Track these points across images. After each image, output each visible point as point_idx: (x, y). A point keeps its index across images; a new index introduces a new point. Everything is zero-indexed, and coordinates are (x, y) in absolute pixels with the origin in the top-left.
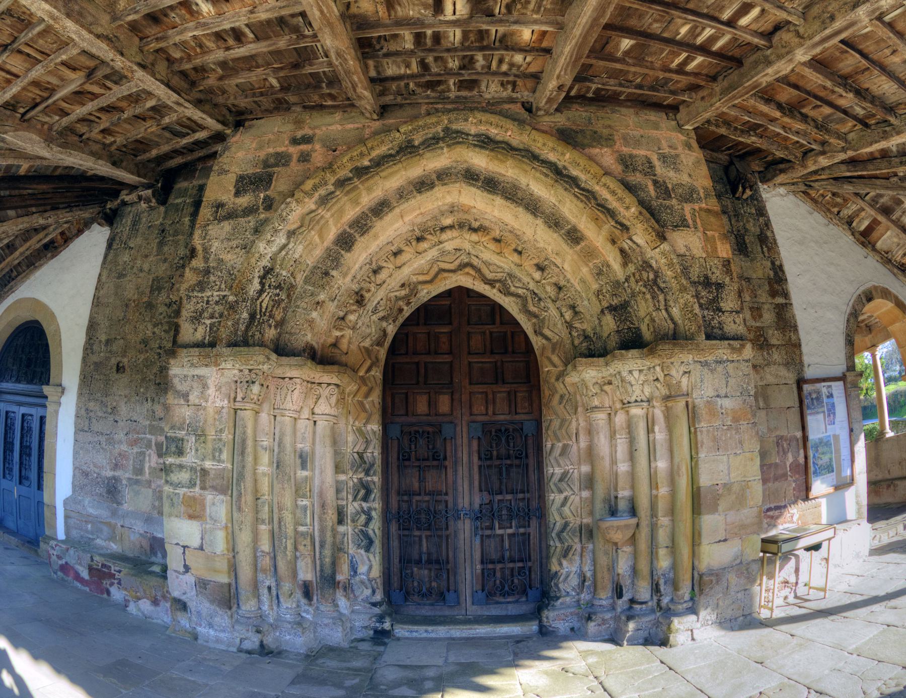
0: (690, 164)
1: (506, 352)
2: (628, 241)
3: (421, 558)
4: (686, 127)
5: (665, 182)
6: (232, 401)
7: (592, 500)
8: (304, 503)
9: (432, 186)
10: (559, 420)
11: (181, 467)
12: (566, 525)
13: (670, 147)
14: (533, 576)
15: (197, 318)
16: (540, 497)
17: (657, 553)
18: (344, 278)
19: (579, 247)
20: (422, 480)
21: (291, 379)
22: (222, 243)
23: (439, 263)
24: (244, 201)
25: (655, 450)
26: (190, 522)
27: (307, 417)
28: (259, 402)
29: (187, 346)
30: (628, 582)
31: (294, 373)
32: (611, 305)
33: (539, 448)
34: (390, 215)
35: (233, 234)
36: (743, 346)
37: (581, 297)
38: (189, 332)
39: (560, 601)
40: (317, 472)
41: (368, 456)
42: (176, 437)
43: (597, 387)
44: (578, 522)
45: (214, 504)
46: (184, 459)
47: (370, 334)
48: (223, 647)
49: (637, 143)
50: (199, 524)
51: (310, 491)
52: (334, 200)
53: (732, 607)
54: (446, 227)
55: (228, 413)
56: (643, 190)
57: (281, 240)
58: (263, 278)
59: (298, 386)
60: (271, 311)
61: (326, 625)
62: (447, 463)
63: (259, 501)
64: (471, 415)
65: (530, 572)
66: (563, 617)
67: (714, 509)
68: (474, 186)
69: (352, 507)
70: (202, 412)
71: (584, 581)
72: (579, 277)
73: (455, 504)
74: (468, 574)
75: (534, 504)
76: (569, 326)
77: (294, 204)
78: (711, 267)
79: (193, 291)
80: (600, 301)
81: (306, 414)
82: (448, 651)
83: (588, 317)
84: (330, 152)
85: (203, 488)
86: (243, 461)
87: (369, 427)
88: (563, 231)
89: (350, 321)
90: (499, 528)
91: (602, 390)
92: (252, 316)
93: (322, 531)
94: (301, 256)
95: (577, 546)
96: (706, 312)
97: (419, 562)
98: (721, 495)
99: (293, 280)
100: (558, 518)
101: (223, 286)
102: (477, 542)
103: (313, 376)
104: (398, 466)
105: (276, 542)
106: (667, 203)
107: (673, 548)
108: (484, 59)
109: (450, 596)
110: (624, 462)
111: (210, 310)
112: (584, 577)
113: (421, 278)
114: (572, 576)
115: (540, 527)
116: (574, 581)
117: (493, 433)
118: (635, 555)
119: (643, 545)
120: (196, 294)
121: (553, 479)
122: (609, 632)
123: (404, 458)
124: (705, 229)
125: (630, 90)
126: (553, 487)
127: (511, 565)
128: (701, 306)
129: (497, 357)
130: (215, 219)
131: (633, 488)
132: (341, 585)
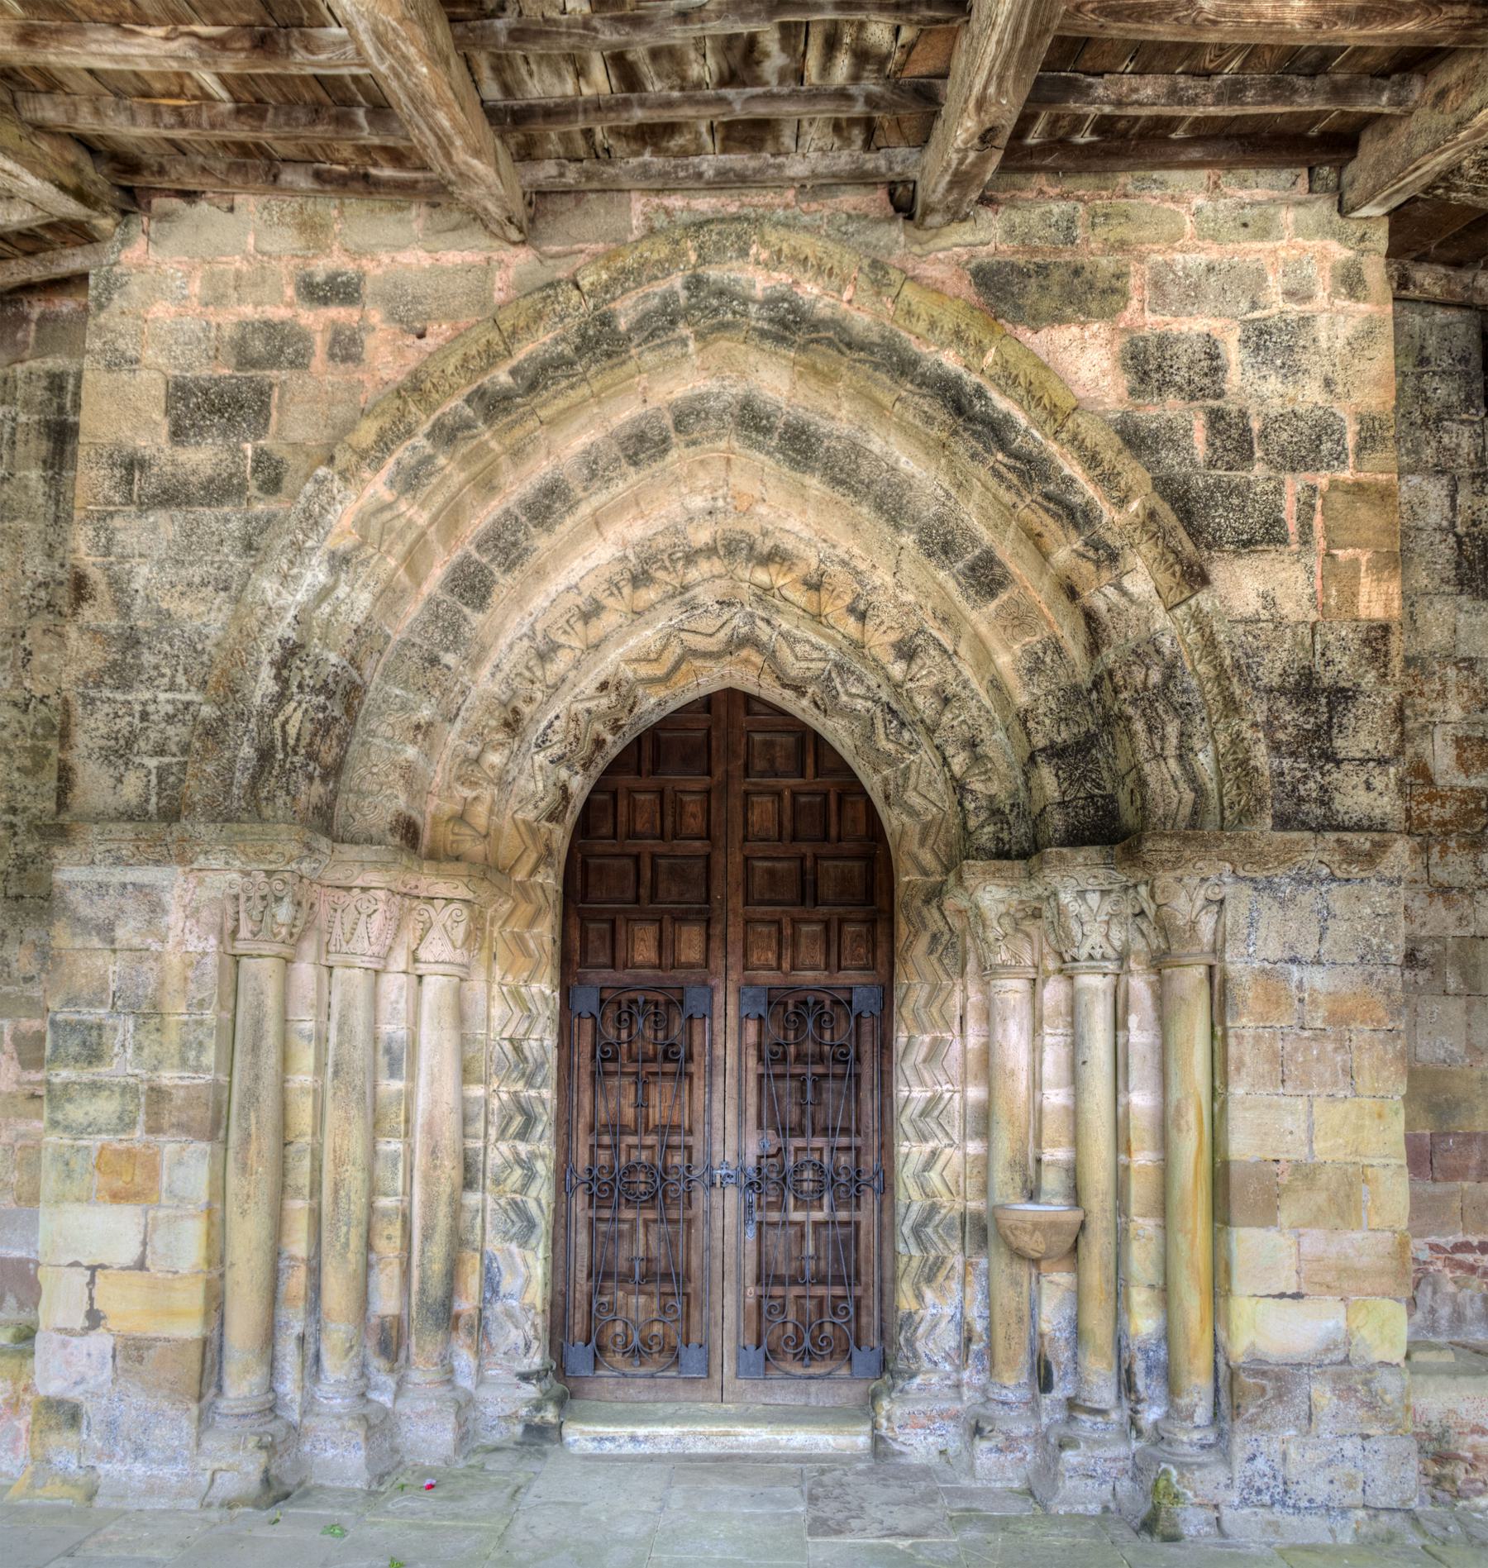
0: (1339, 344)
1: (826, 837)
2: (1110, 591)
3: (632, 1269)
4: (1365, 212)
5: (1243, 414)
6: (227, 938)
7: (985, 1163)
8: (392, 1147)
9: (662, 446)
10: (927, 988)
11: (95, 1087)
12: (933, 1209)
13: (1290, 294)
14: (864, 1320)
15: (119, 751)
16: (882, 1146)
17: (1128, 1297)
18: (474, 669)
19: (993, 605)
20: (642, 1104)
21: (364, 889)
22: (162, 569)
23: (683, 635)
24: (201, 457)
25: (1127, 1065)
26: (115, 1207)
27: (403, 967)
28: (295, 939)
29: (99, 818)
30: (1065, 1355)
31: (372, 878)
32: (1053, 744)
33: (885, 1043)
34: (569, 521)
35: (188, 549)
36: (1382, 847)
37: (991, 722)
38: (95, 785)
39: (918, 1380)
40: (423, 1080)
41: (531, 1047)
42: (81, 1023)
43: (1006, 921)
44: (958, 1207)
45: (180, 1163)
46: (102, 1070)
47: (534, 794)
48: (162, 1504)
49: (1193, 295)
50: (138, 1210)
51: (407, 1121)
52: (434, 480)
53: (1330, 1473)
54: (698, 552)
55: (221, 967)
56: (1174, 444)
57: (316, 574)
58: (281, 666)
59: (381, 906)
60: (311, 744)
61: (420, 1416)
62: (693, 1068)
63: (292, 1148)
64: (745, 968)
65: (858, 1308)
66: (923, 1420)
67: (1266, 1215)
68: (759, 447)
69: (499, 1153)
70: (152, 964)
71: (969, 1340)
72: (988, 677)
73: (710, 1155)
74: (728, 1308)
75: (870, 1161)
76: (959, 787)
77: (337, 483)
78: (1327, 646)
79: (98, 685)
80: (1028, 734)
81: (400, 960)
82: (670, 1485)
83: (1003, 769)
84: (411, 339)
85: (154, 1129)
86: (255, 1065)
87: (535, 988)
88: (960, 565)
89: (493, 767)
90: (796, 1209)
91: (1017, 930)
92: (265, 755)
93: (430, 1204)
94: (369, 619)
95: (956, 1261)
96: (1287, 763)
97: (626, 1278)
98: (1288, 1188)
99: (355, 673)
100: (915, 1194)
101: (181, 679)
102: (751, 1234)
103: (413, 883)
104: (593, 1074)
105: (325, 1235)
106: (1237, 476)
107: (1165, 1293)
108: (783, 49)
109: (691, 1357)
110: (1058, 1086)
111: (153, 735)
112: (970, 1331)
113: (645, 671)
114: (943, 1324)
115: (881, 1211)
116: (949, 1338)
117: (791, 1008)
118: (1078, 1295)
119: (1096, 1273)
120: (106, 693)
121: (908, 1111)
122: (1022, 1472)
123: (605, 1057)
124: (1332, 544)
125: (1199, 111)
126: (907, 1127)
127: (820, 1291)
128: (1275, 747)
129: (806, 848)
130: (129, 501)
131: (1076, 1142)
132: (462, 1322)
